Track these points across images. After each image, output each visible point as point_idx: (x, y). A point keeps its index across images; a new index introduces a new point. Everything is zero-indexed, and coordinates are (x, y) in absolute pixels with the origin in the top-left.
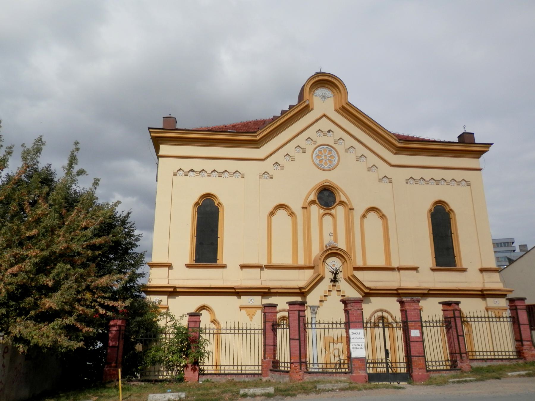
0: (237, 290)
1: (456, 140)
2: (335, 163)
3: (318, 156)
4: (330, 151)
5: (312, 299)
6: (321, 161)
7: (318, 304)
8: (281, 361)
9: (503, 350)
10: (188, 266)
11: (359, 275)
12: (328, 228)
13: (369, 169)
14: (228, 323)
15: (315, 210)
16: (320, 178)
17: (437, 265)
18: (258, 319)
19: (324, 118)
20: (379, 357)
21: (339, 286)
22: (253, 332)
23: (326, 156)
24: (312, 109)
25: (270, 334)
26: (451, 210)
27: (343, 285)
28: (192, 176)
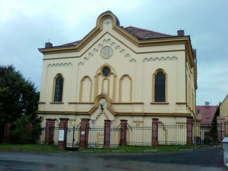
0: (174, 115)
2: (110, 55)
5: (93, 117)
7: (95, 119)
9: (137, 142)
10: (51, 103)
12: (106, 86)
13: (126, 56)
14: (170, 123)
15: (101, 78)
16: (103, 62)
17: (155, 101)
23: (107, 52)
24: (102, 30)
27: (106, 111)
28: (54, 67)
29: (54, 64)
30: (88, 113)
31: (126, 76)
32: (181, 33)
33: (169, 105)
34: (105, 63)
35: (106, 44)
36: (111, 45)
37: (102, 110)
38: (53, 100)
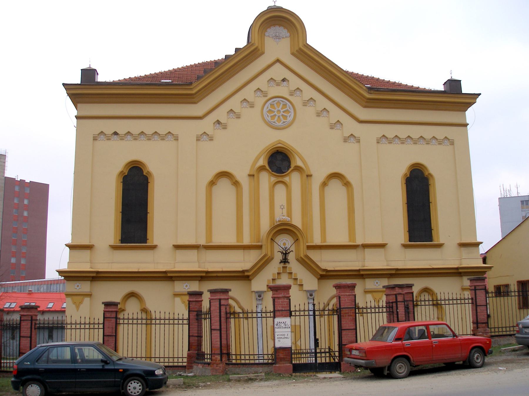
0: (169, 275)
1: (441, 88)
3: (270, 111)
4: (285, 105)
6: (273, 117)
8: (206, 353)
11: (315, 256)
12: (281, 200)
13: (332, 127)
15: (266, 179)
16: (271, 138)
18: (181, 310)
19: (278, 65)
20: (308, 347)
21: (290, 268)
22: (140, 322)
23: (280, 110)
24: (263, 53)
25: (195, 324)
26: (430, 174)
28: (115, 143)
29: (116, 133)
30: (246, 274)
31: (336, 176)
32: (453, 85)
33: (156, 250)
34: (276, 140)
35: (274, 91)
36: (292, 94)
37: (282, 265)
38: (119, 237)
